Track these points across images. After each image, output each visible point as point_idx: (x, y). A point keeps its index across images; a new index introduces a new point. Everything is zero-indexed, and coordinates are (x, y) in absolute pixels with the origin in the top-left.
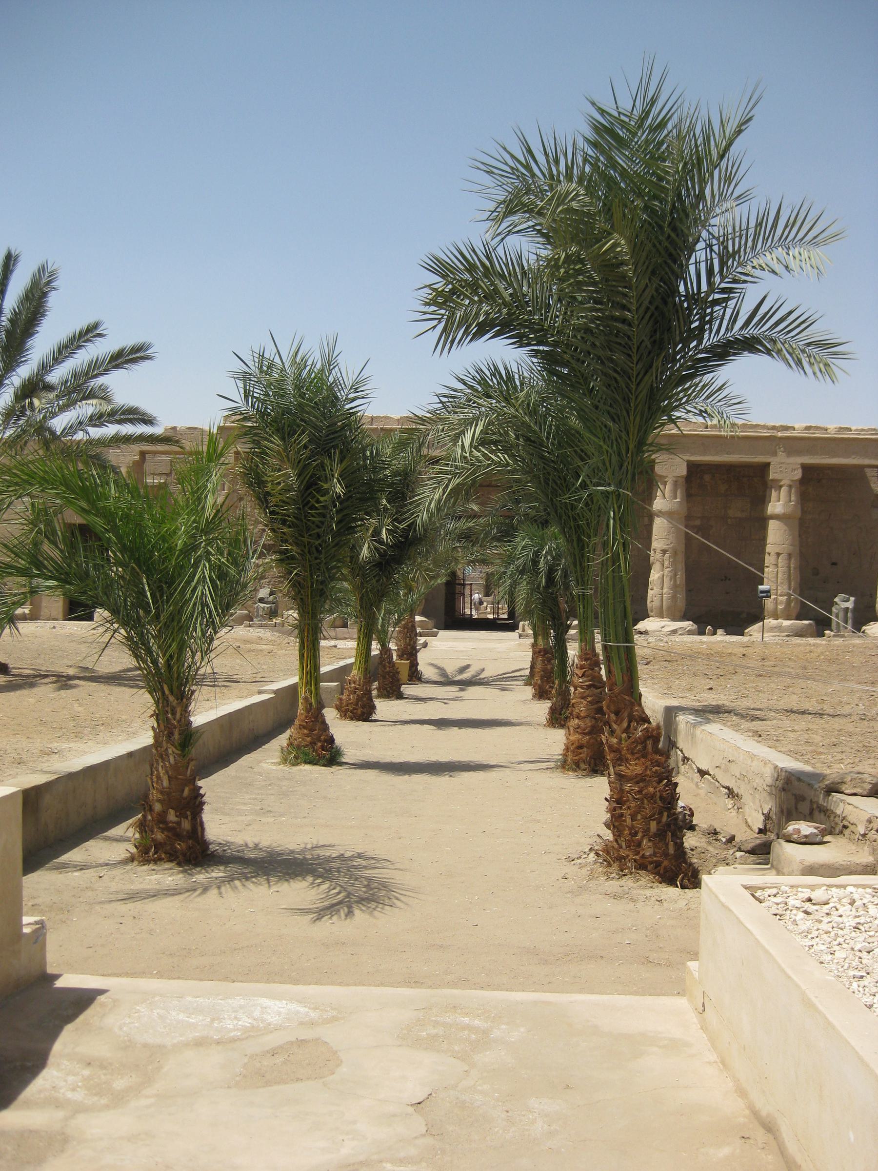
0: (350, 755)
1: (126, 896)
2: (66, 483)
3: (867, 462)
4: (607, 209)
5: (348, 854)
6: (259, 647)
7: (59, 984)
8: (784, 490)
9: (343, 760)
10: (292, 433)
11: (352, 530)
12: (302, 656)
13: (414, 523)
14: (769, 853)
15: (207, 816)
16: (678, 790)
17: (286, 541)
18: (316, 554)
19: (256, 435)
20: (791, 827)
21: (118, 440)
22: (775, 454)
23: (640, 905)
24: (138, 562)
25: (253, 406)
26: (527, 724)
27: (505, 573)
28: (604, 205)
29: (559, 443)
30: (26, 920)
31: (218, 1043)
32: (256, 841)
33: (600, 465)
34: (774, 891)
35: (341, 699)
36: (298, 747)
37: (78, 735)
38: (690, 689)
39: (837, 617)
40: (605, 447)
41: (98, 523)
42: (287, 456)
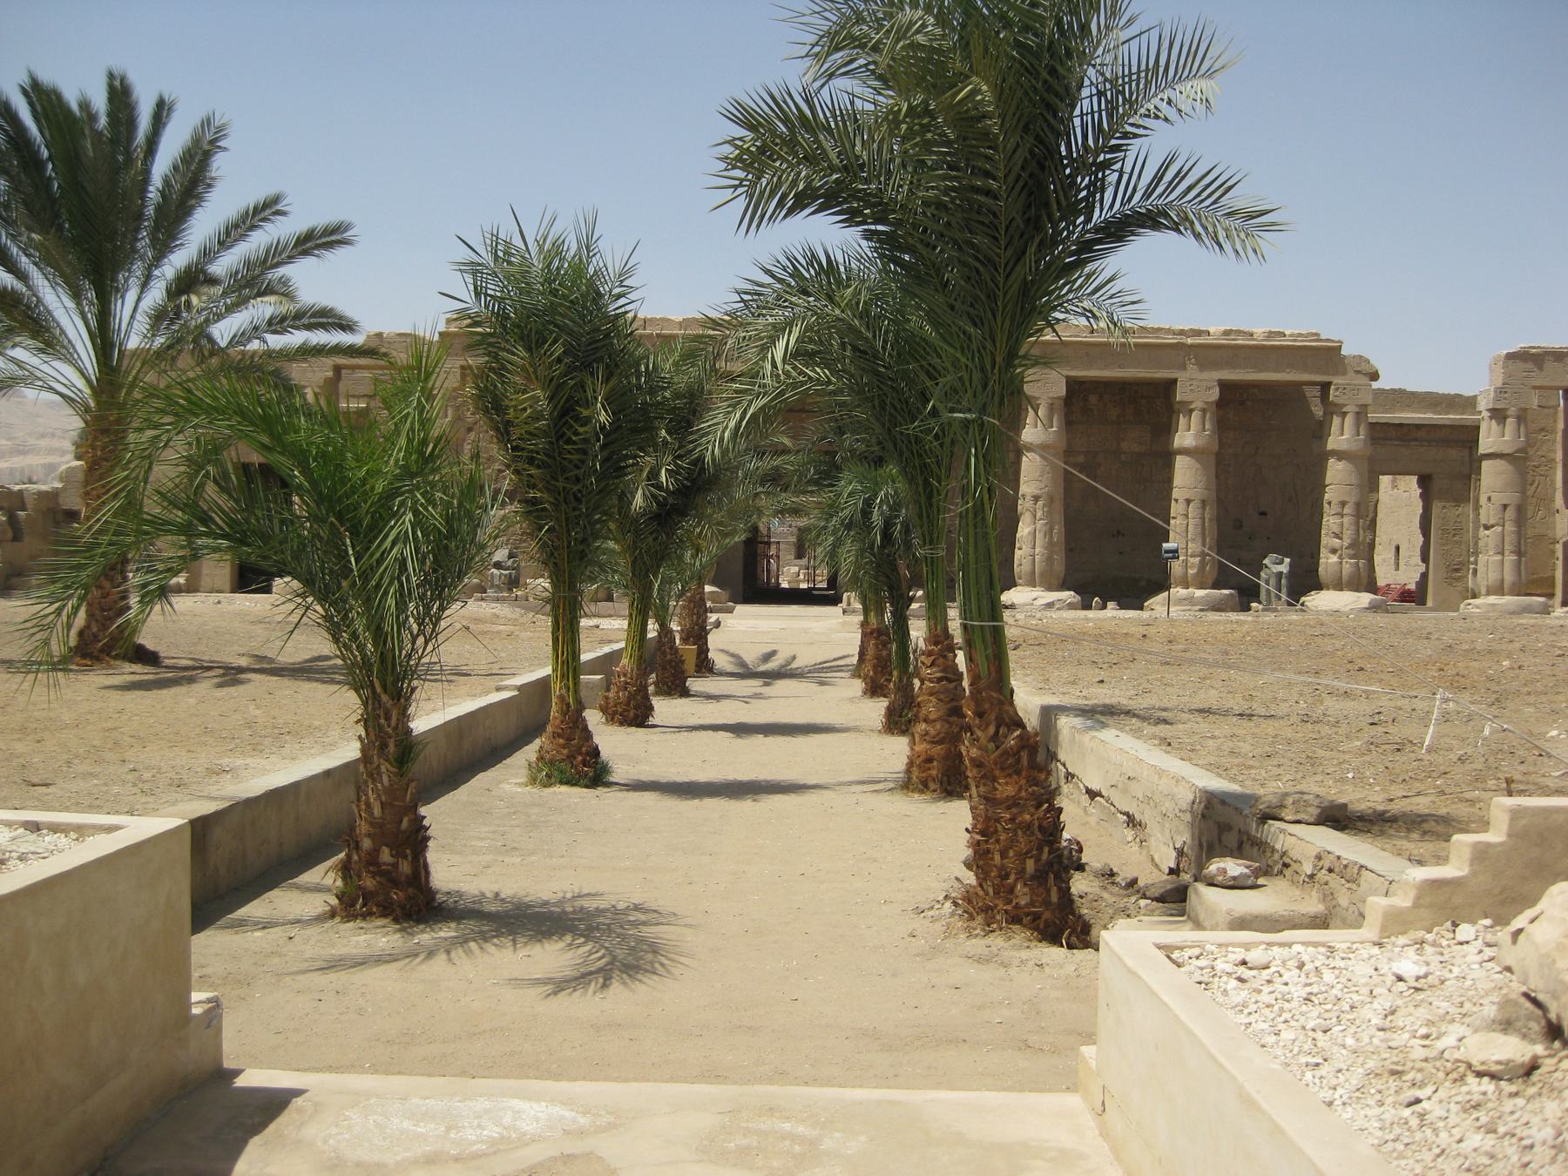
0: (621, 771)
1: (324, 965)
2: (241, 412)
3: (1306, 377)
4: (965, 44)
5: (621, 906)
6: (495, 628)
7: (240, 1082)
8: (1195, 416)
9: (612, 779)
10: (541, 341)
11: (620, 471)
12: (555, 640)
13: (701, 459)
14: (1184, 900)
15: (432, 855)
16: (1062, 818)
17: (534, 487)
18: (575, 504)
19: (490, 344)
20: (1214, 867)
21: (308, 352)
22: (1183, 367)
23: (1013, 971)
24: (340, 517)
25: (487, 307)
26: (856, 729)
27: (825, 528)
28: (961, 37)
29: (899, 354)
30: (196, 996)
31: (457, 1159)
32: (495, 888)
33: (958, 385)
34: (1196, 951)
35: (607, 698)
36: (552, 763)
37: (256, 748)
38: (1074, 683)
39: (1267, 582)
40: (964, 360)
41: (282, 462)
42: (535, 372)
